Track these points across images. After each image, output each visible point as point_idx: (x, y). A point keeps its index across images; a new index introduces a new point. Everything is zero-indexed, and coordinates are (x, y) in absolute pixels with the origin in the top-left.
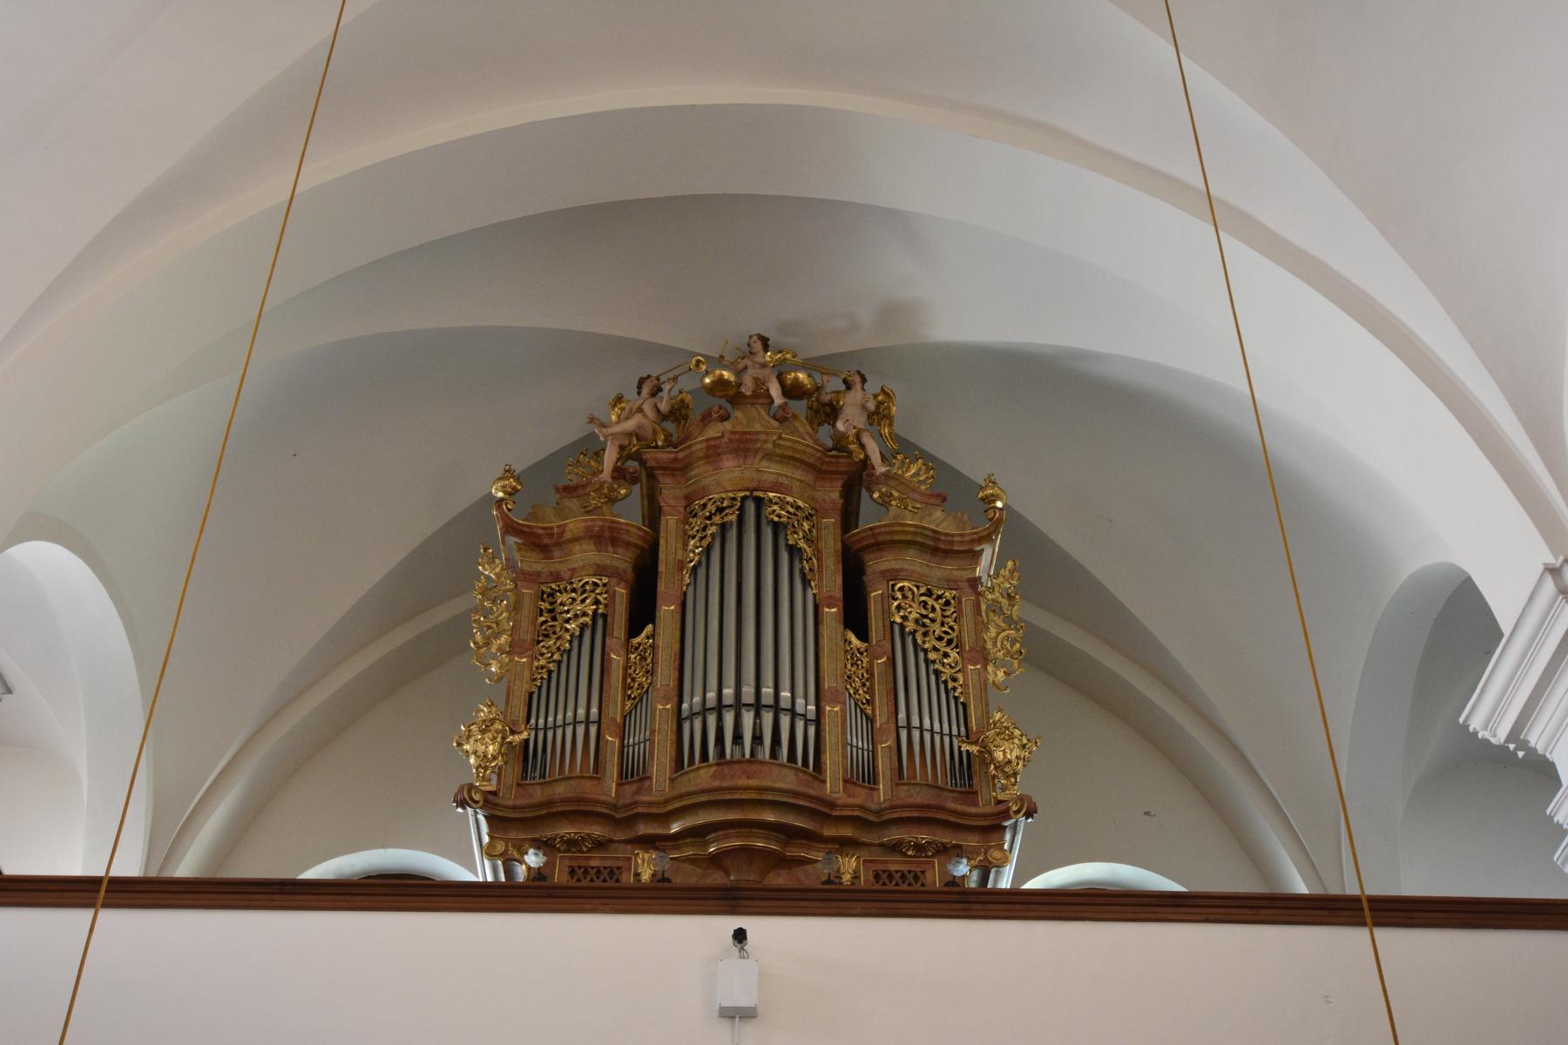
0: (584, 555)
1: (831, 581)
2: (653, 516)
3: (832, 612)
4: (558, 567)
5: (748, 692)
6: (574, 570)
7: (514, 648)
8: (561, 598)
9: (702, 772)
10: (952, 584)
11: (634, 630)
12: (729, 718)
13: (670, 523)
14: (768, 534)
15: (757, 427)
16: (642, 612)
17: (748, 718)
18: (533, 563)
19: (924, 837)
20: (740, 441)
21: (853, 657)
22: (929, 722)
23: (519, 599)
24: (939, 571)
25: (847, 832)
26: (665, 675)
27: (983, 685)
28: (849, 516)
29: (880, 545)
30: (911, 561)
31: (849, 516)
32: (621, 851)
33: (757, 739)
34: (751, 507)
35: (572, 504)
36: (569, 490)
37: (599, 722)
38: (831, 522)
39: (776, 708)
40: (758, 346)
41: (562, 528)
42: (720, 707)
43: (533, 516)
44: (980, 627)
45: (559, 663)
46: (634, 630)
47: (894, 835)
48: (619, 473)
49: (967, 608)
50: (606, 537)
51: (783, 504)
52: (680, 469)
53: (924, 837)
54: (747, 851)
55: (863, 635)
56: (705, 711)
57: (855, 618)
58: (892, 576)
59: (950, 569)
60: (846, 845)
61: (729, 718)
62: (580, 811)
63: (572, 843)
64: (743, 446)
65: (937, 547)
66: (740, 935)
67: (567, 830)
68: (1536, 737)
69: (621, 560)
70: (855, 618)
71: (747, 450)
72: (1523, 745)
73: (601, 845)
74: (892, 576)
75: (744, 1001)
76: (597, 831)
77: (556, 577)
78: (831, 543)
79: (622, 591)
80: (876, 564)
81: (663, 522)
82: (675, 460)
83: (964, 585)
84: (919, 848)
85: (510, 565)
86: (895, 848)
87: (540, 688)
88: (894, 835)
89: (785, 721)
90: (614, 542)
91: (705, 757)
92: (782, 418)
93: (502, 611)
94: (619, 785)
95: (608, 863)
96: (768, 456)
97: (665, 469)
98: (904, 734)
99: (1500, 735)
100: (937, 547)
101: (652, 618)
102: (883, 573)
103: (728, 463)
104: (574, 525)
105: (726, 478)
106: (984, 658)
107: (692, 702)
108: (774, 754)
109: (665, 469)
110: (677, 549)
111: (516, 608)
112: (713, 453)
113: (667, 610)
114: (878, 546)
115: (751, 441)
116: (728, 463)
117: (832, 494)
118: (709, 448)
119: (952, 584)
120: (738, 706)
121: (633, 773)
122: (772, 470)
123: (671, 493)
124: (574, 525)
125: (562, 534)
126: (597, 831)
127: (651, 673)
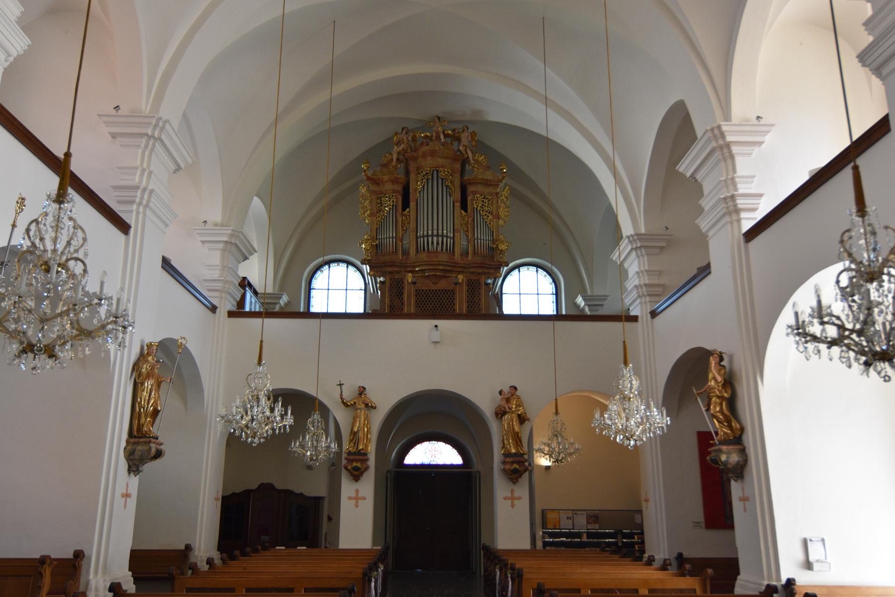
0: (389, 186)
1: (458, 195)
2: (407, 173)
3: (458, 204)
5: (435, 232)
7: (371, 215)
8: (383, 199)
10: (491, 194)
11: (404, 210)
12: (430, 239)
13: (412, 176)
14: (440, 181)
15: (437, 148)
16: (406, 204)
17: (435, 239)
18: (374, 188)
19: (480, 271)
21: (463, 218)
22: (483, 237)
24: (487, 190)
25: (461, 270)
26: (413, 218)
27: (498, 225)
28: (463, 172)
29: (472, 183)
30: (480, 188)
31: (463, 172)
33: (438, 243)
34: (435, 172)
35: (385, 170)
36: (384, 166)
38: (458, 175)
39: (443, 236)
40: (437, 120)
42: (428, 236)
43: (374, 174)
44: (498, 208)
46: (404, 210)
47: (471, 270)
48: (398, 159)
49: (495, 202)
50: (394, 181)
51: (444, 172)
52: (415, 159)
53: (480, 271)
54: (436, 275)
55: (466, 211)
56: (424, 236)
57: (464, 207)
58: (474, 193)
59: (491, 189)
60: (460, 272)
61: (430, 239)
62: (392, 264)
63: (391, 273)
64: (433, 154)
65: (487, 183)
66: (436, 326)
67: (389, 269)
68: (699, 177)
69: (399, 188)
70: (464, 207)
72: (695, 178)
73: (398, 272)
74: (474, 193)
75: (438, 340)
76: (396, 269)
77: (382, 193)
78: (457, 182)
79: (400, 198)
80: (471, 189)
84: (479, 274)
85: (368, 189)
86: (473, 273)
88: (471, 270)
89: (445, 239)
90: (397, 183)
92: (443, 144)
93: (367, 203)
96: (440, 157)
99: (688, 174)
100: (487, 183)
101: (408, 206)
103: (429, 158)
104: (386, 178)
105: (428, 163)
106: (498, 217)
107: (420, 233)
110: (417, 185)
111: (371, 202)
112: (424, 156)
114: (471, 184)
116: (429, 158)
117: (458, 166)
119: (491, 194)
120: (432, 236)
121: (406, 253)
122: (441, 161)
123: (412, 166)
124: (386, 178)
126: (396, 269)
127: (409, 223)
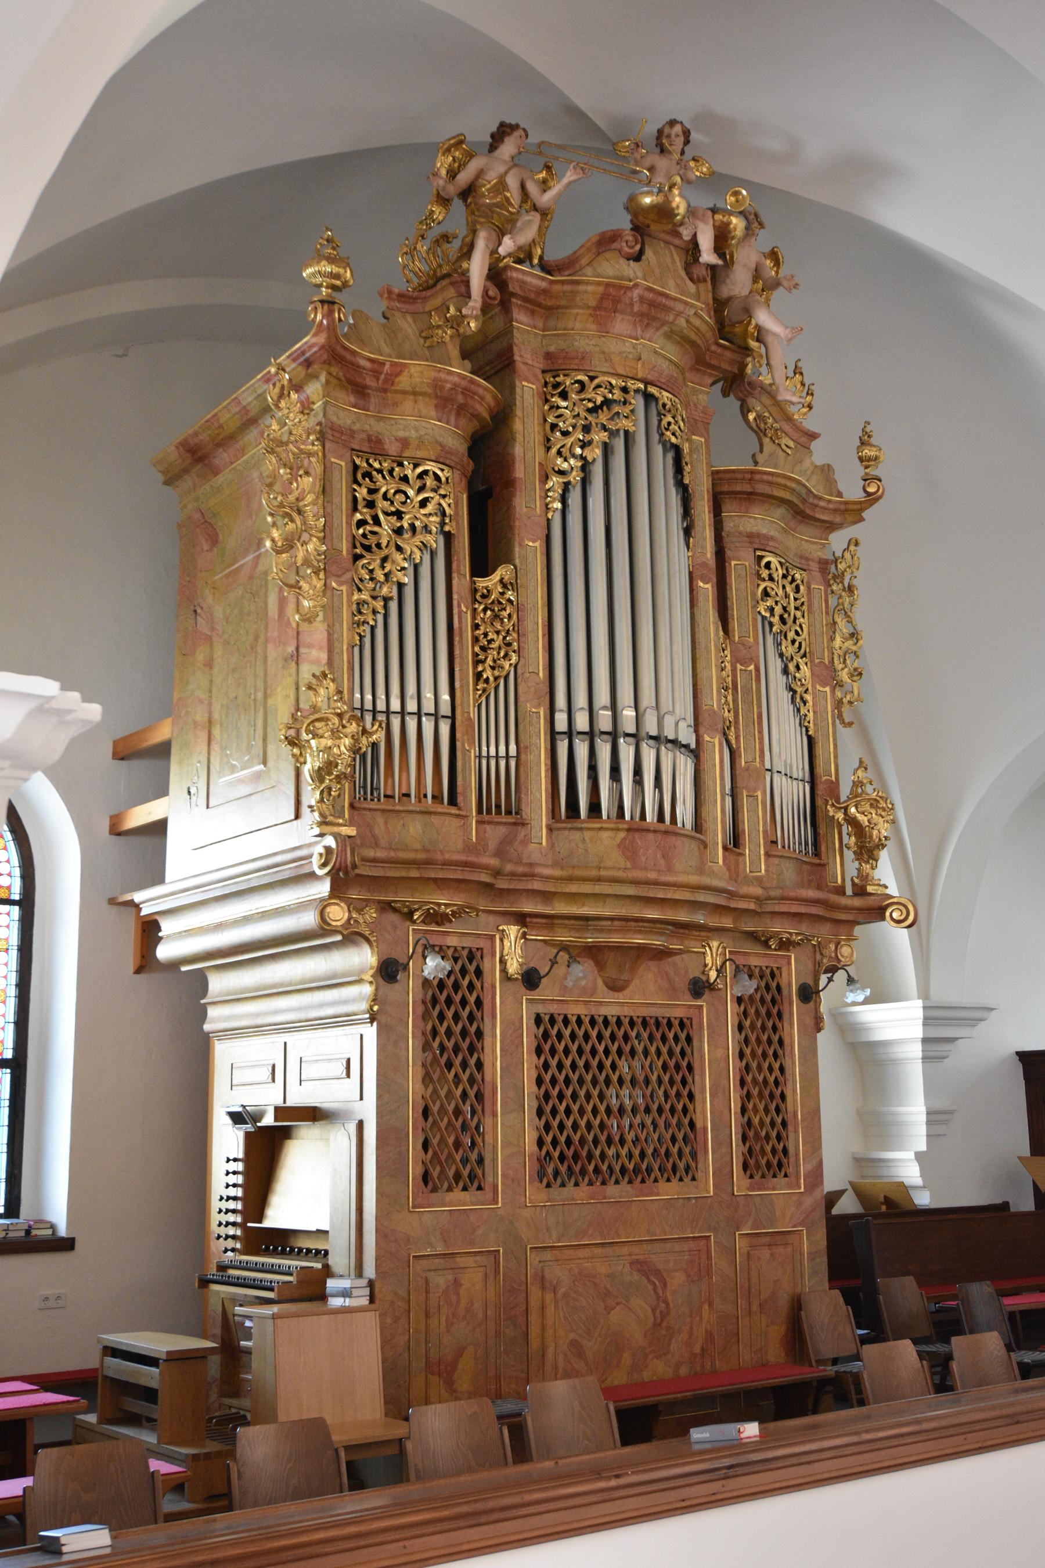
4: (376, 427)
6: (405, 443)
9: (605, 835)
11: (481, 567)
18: (348, 414)
20: (652, 304)
23: (327, 469)
32: (485, 923)
37: (453, 717)
41: (399, 370)
45: (386, 600)
71: (655, 319)
81: (518, 390)
82: (545, 292)
83: (814, 566)
87: (373, 628)
91: (595, 808)
94: (550, 829)
95: (468, 943)
97: (526, 300)
98: (484, 762)
102: (751, 536)
108: (784, 847)
109: (526, 300)
113: (528, 547)
115: (668, 309)
118: (604, 297)
125: (391, 379)
